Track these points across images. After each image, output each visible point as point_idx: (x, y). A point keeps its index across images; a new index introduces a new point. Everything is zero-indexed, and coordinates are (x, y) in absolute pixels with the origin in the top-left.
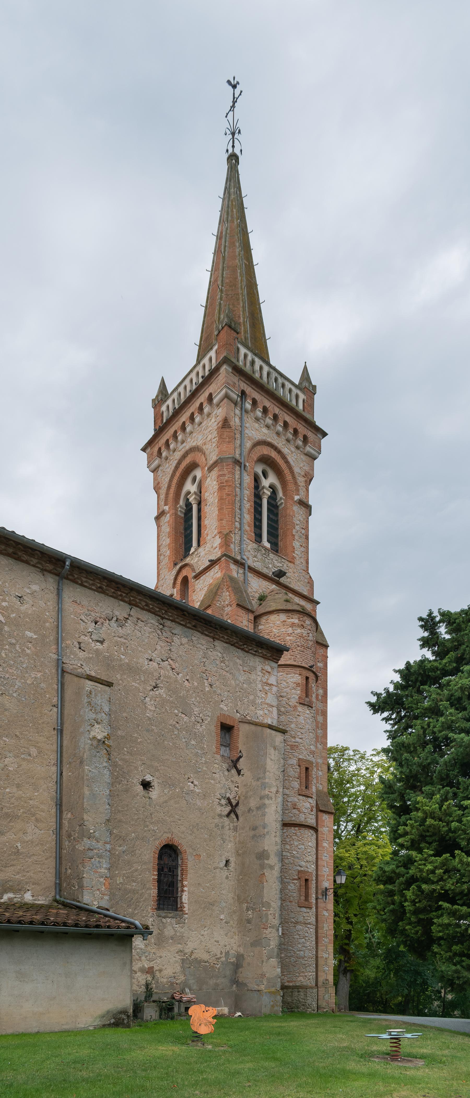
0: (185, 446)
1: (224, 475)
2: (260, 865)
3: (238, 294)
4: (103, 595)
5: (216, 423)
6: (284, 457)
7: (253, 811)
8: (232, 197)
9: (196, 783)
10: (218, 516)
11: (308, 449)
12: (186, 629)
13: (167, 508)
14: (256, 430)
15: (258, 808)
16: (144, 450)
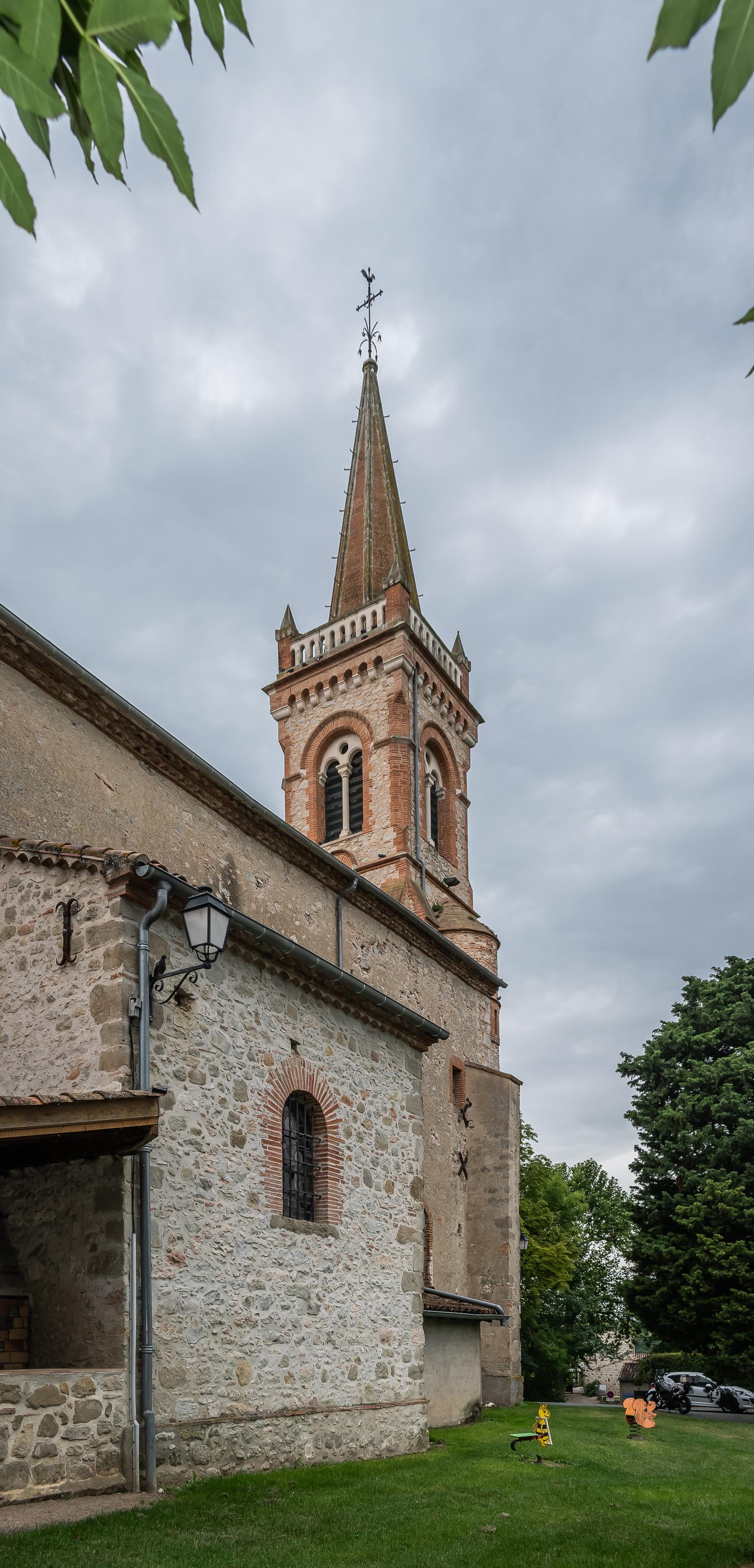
0: (333, 706)
1: (398, 758)
2: (503, 1233)
3: (389, 536)
4: (368, 916)
5: (385, 693)
6: (448, 744)
7: (489, 1171)
8: (374, 414)
9: (437, 1135)
10: (391, 805)
11: (467, 736)
12: (427, 958)
13: (304, 772)
14: (426, 712)
15: (497, 1169)
16: (266, 690)
